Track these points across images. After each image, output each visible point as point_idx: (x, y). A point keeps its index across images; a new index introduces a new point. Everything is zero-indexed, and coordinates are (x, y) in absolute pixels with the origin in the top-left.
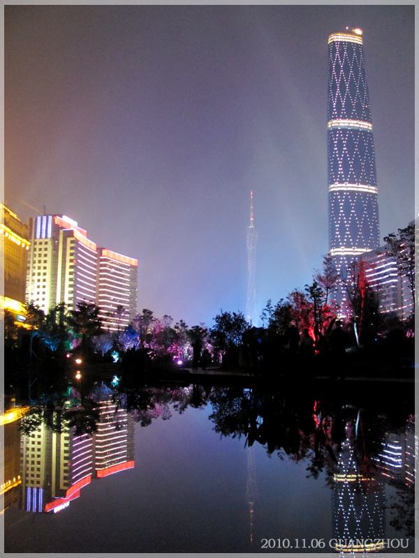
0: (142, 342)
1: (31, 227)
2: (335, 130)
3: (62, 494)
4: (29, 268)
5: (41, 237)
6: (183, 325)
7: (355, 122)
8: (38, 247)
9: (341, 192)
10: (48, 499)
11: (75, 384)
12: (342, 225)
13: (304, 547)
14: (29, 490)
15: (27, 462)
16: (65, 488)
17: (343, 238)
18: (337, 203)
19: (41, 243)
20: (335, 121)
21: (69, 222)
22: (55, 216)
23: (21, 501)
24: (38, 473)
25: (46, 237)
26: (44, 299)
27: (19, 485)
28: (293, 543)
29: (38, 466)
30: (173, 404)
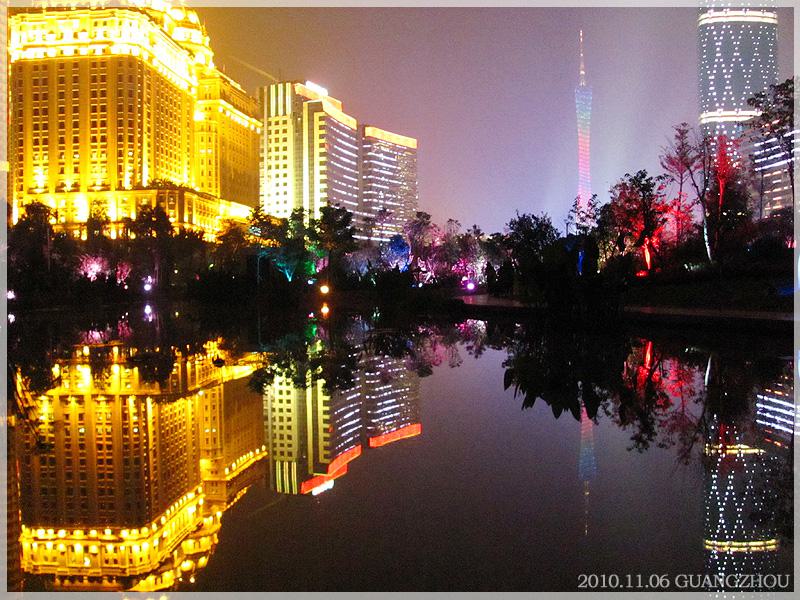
0: (415, 259)
1: (263, 101)
3: (324, 469)
4: (262, 159)
5: (277, 115)
6: (478, 232)
8: (273, 128)
9: (718, 26)
10: (304, 476)
11: (320, 320)
14: (278, 465)
15: (274, 427)
16: (326, 461)
17: (719, 97)
18: (711, 43)
19: (277, 123)
21: (315, 90)
22: (296, 82)
23: (268, 479)
24: (288, 432)
25: (285, 114)
26: (285, 175)
27: (264, 458)
29: (290, 449)
30: (465, 345)
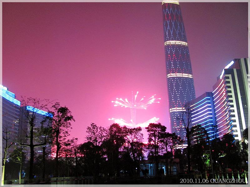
2: (168, 46)
7: (179, 42)
12: (175, 95)
13: (199, 182)
16: (227, 75)
20: (167, 42)
28: (194, 181)
